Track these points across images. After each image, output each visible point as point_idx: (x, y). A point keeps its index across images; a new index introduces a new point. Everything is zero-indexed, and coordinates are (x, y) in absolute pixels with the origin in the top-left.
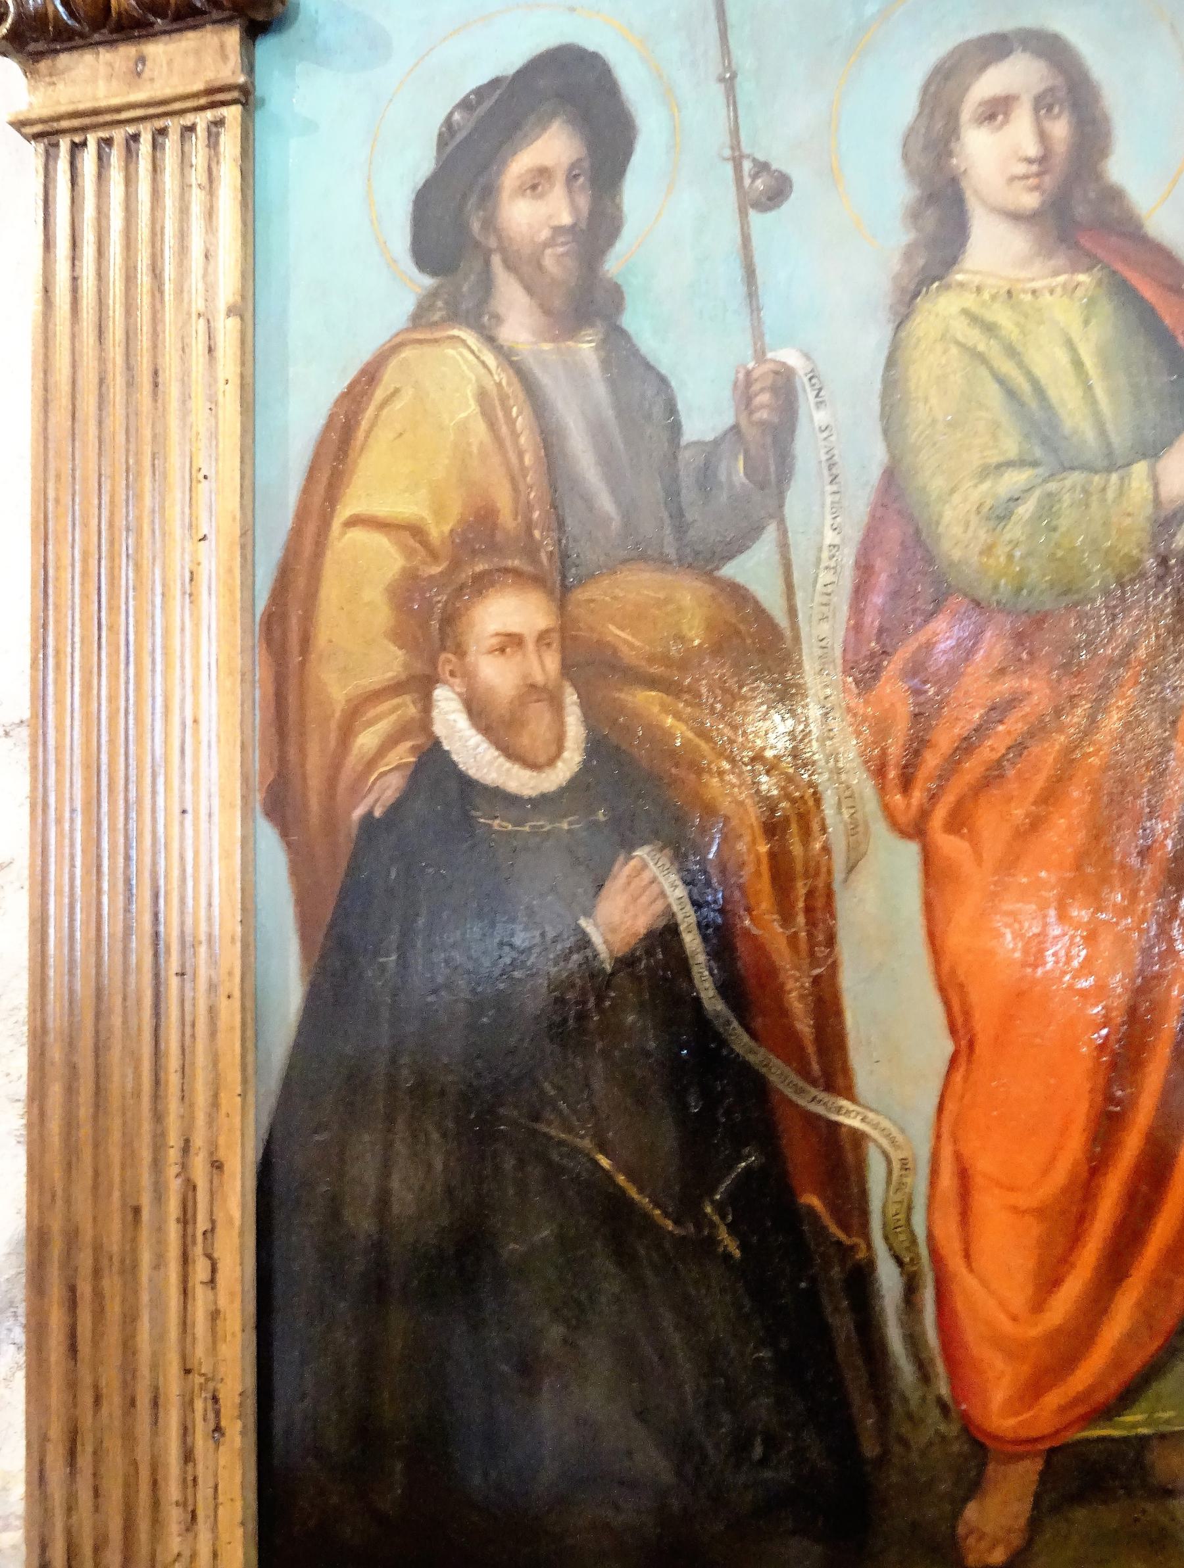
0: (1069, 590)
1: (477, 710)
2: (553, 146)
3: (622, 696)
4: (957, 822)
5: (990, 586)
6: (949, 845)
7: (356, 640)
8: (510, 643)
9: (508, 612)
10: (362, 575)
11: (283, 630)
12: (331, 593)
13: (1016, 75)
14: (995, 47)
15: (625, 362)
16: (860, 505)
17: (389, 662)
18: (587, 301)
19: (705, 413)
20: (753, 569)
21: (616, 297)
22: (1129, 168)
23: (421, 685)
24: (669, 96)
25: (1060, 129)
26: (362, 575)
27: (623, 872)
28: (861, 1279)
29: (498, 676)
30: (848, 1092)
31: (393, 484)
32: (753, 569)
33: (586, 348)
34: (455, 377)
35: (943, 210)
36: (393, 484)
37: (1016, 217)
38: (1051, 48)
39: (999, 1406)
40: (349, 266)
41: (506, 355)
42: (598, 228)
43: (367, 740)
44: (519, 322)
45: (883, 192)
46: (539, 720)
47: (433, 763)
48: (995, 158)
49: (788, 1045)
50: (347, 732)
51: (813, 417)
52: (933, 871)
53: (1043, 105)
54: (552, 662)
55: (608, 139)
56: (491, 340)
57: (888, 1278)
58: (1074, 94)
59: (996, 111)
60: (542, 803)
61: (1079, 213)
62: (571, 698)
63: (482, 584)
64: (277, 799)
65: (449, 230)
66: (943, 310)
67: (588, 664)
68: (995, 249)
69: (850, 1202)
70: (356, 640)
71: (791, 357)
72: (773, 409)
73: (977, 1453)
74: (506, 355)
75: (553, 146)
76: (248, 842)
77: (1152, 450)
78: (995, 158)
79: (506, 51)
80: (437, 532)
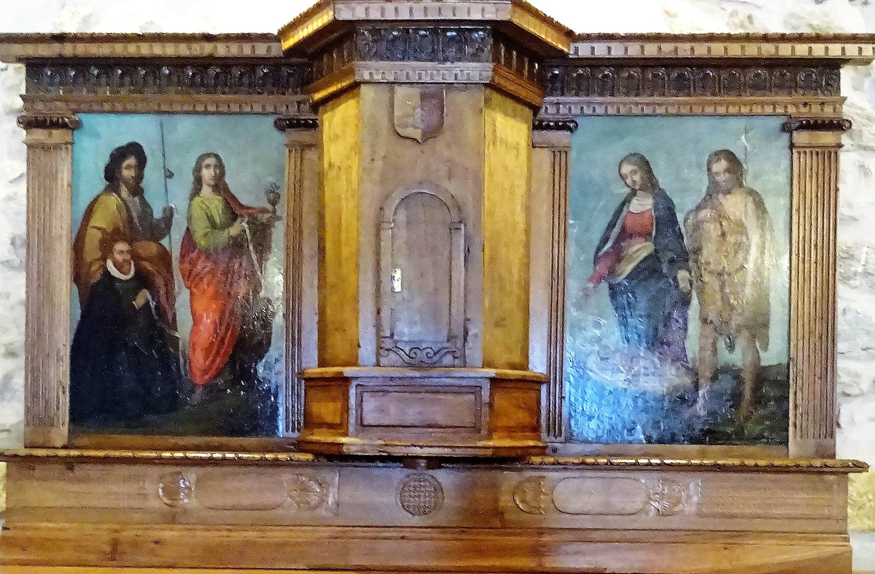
0: (216, 250)
1: (116, 264)
2: (131, 161)
3: (199, 360)
4: (196, 286)
5: (349, 346)
6: (195, 290)
7: (92, 250)
8: (122, 252)
9: (121, 246)
10: (93, 238)
11: (78, 247)
12: (88, 239)
13: (211, 161)
14: (208, 155)
15: (145, 204)
16: (183, 234)
17: (98, 255)
18: (137, 190)
19: (158, 214)
20: (165, 242)
21: (142, 190)
22: (228, 180)
23: (104, 259)
24: (153, 156)
25: (218, 171)
26: (93, 238)
27: (140, 294)
28: (178, 359)
29: (119, 258)
30: (176, 330)
31: (99, 220)
32: (165, 242)
33: (137, 199)
34: (113, 200)
35: (198, 181)
36: (99, 220)
37: (209, 185)
38: (217, 156)
39: (199, 380)
40: (93, 182)
41: (122, 199)
42: (139, 177)
43: (94, 268)
44: (124, 192)
45: (189, 178)
46: (126, 267)
47: (107, 273)
48: (207, 174)
49: (167, 323)
50: (90, 267)
51: (176, 216)
52: (191, 294)
53: (215, 167)
54: (129, 257)
55: (142, 161)
56: (120, 197)
57: (182, 361)
58: (220, 166)
59: (208, 166)
60: (127, 281)
61: (219, 186)
62: (132, 263)
63: (116, 241)
64: (77, 277)
65: (112, 174)
66: (197, 200)
67: (136, 257)
68: (206, 191)
69: (176, 347)
70: (92, 250)
71: (173, 206)
72: (169, 214)
73: (195, 385)
74: (122, 199)
75: (131, 161)
76: (71, 287)
77: (813, 458)
78: (207, 174)
79: (123, 141)
80: (109, 231)
